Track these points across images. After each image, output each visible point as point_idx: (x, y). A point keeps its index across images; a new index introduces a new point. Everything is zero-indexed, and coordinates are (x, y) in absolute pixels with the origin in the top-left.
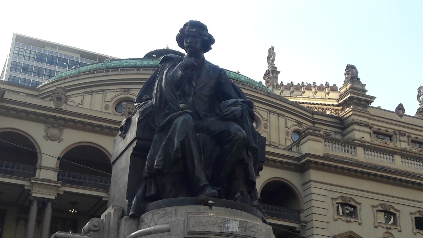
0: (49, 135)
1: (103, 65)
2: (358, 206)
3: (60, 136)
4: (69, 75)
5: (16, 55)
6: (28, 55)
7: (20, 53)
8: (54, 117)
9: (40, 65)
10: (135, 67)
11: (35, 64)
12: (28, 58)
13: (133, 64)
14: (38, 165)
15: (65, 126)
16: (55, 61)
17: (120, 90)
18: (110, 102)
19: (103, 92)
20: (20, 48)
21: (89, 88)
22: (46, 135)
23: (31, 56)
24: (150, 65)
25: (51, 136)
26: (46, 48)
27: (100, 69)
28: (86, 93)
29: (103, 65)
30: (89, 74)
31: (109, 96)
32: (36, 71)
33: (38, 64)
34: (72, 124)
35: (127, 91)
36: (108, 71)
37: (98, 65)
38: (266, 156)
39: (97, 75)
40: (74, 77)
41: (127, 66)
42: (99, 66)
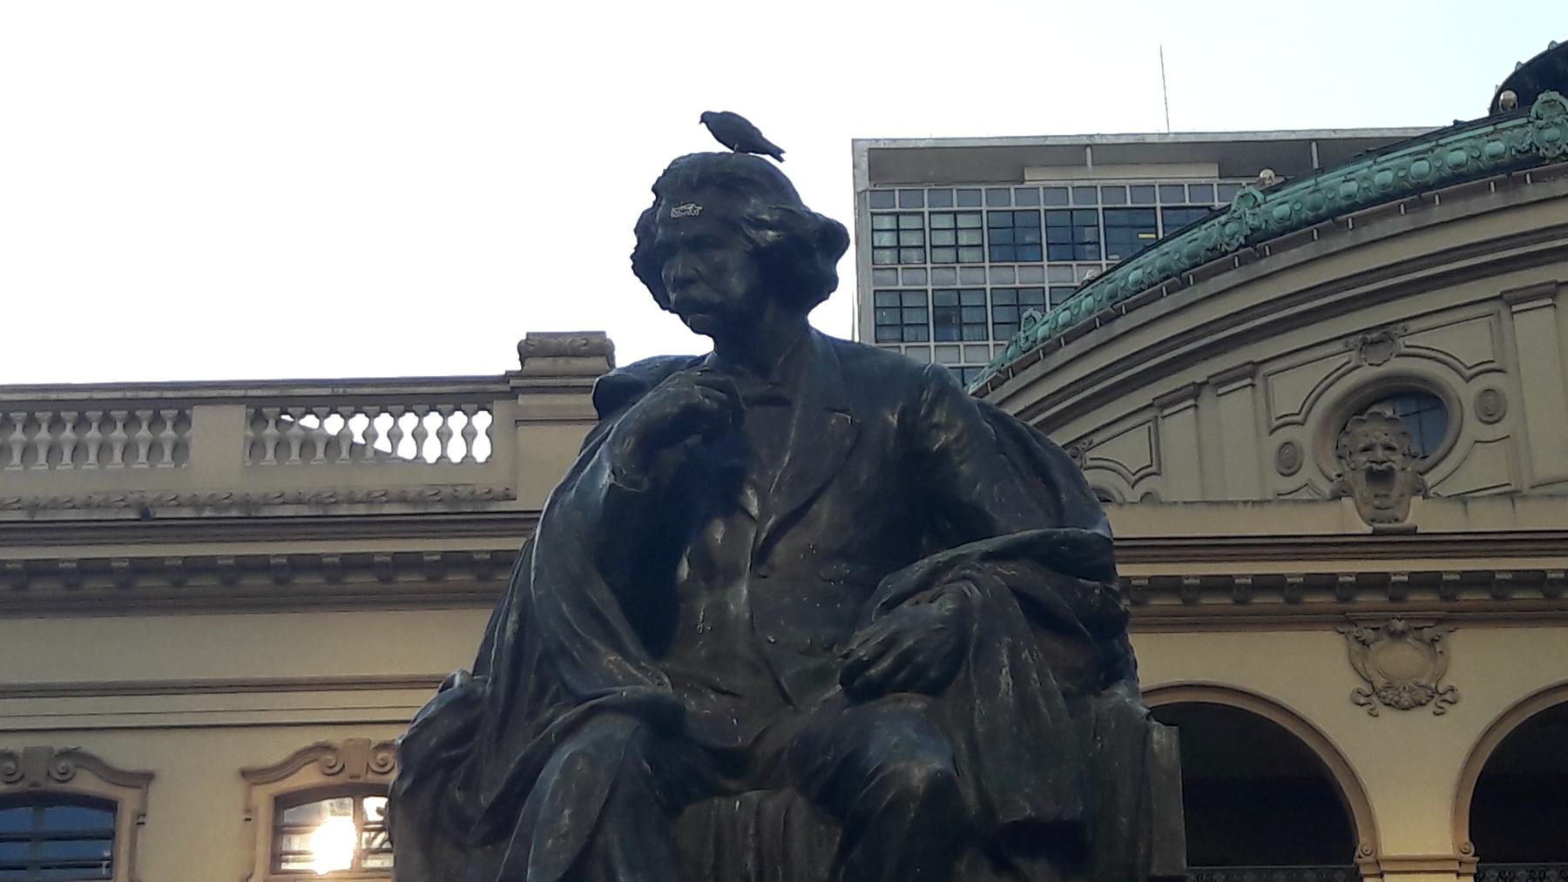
0: (1380, 682)
1: (1229, 229)
2: (129, 800)
3: (1439, 678)
4: (1065, 325)
5: (887, 257)
6: (948, 238)
7: (907, 239)
8: (1379, 583)
9: (1019, 276)
10: (1404, 193)
11: (991, 278)
12: (949, 255)
13: (1388, 177)
14: (1362, 857)
15: (1453, 619)
16: (1089, 234)
17: (1339, 346)
18: (1302, 424)
19: (1252, 375)
20: (897, 215)
21: (1171, 374)
22: (1367, 689)
23: (964, 239)
24: (1485, 163)
25: (1389, 686)
26: (1036, 178)
27: (1215, 252)
28: (1163, 404)
29: (1229, 229)
30: (1158, 296)
31: (1290, 391)
32: (1004, 315)
33: (1005, 274)
34: (1172, 602)
35: (1378, 339)
36: (1426, 203)
37: (1199, 233)
38: (1123, 570)
39: (1200, 291)
40: (1089, 328)
41: (1430, 180)
42: (1208, 237)
